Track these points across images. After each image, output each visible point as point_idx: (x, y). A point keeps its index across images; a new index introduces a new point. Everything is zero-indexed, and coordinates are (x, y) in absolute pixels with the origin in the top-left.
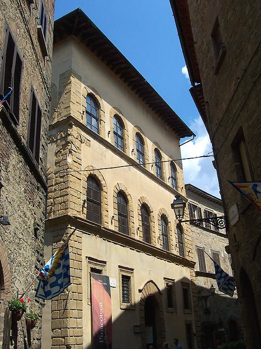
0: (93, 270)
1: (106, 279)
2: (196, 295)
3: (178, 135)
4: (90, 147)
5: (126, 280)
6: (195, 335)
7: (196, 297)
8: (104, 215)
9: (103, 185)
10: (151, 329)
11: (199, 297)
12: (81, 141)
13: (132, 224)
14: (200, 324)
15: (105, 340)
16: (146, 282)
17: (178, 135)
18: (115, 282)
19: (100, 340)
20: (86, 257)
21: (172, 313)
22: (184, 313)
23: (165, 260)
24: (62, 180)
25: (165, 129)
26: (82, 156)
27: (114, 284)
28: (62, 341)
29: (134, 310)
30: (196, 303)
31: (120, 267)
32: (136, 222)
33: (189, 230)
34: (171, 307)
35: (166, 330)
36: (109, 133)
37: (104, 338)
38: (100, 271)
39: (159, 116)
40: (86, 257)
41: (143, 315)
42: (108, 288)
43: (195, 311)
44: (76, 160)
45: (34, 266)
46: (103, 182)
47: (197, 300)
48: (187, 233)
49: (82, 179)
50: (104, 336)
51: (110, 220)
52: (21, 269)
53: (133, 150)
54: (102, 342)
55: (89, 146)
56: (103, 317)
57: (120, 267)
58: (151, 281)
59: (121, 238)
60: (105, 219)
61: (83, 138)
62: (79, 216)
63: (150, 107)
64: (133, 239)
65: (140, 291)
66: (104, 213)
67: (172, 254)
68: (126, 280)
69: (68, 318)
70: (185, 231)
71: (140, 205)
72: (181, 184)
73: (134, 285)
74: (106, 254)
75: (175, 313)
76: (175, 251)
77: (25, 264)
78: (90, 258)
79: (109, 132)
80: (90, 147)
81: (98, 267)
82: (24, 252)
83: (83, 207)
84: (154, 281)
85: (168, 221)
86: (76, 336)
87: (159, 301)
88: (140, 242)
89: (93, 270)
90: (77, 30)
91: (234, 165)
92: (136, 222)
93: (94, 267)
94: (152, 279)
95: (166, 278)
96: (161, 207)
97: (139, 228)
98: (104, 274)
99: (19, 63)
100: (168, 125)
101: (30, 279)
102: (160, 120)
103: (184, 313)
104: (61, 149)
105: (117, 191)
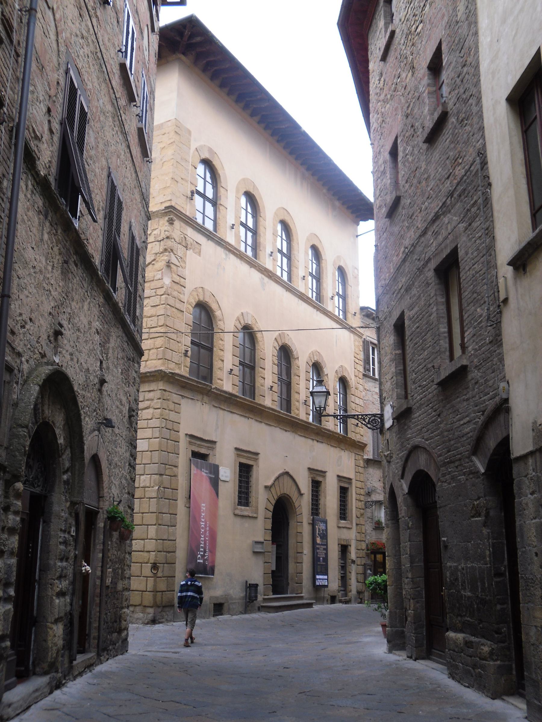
0: (195, 455)
1: (215, 470)
2: (362, 498)
4: (200, 255)
5: (245, 471)
6: (353, 562)
7: (361, 501)
8: (217, 367)
9: (218, 319)
11: (366, 502)
12: (186, 247)
13: (262, 381)
14: (364, 546)
15: (206, 560)
16: (277, 475)
17: (357, 217)
18: (227, 473)
19: (199, 559)
20: (186, 434)
22: (339, 527)
23: (313, 440)
25: (334, 208)
27: (226, 477)
29: (256, 518)
30: (362, 511)
32: (268, 374)
33: (361, 388)
37: (203, 556)
41: (269, 526)
42: (215, 482)
43: (357, 525)
44: (177, 279)
45: (127, 464)
46: (218, 313)
47: (363, 507)
48: (357, 393)
49: (184, 310)
50: (204, 554)
51: (226, 380)
52: (117, 471)
53: (272, 253)
54: (202, 561)
55: (199, 254)
58: (287, 473)
59: (244, 403)
60: (217, 373)
61: (189, 241)
62: (177, 371)
64: (260, 405)
66: (217, 364)
67: (325, 429)
68: (245, 471)
70: (353, 390)
72: (353, 308)
73: (257, 480)
77: (120, 464)
78: (192, 436)
79: (233, 225)
80: (200, 255)
81: (203, 451)
82: (120, 449)
83: (186, 354)
84: (291, 473)
85: (323, 372)
87: (296, 505)
88: (273, 410)
89: (195, 455)
90: (191, 47)
91: (394, 353)
92: (268, 374)
93: (196, 449)
94: (287, 470)
95: (313, 470)
96: (313, 349)
97: (272, 387)
98: (211, 460)
99: (120, 203)
101: (124, 481)
103: (339, 527)
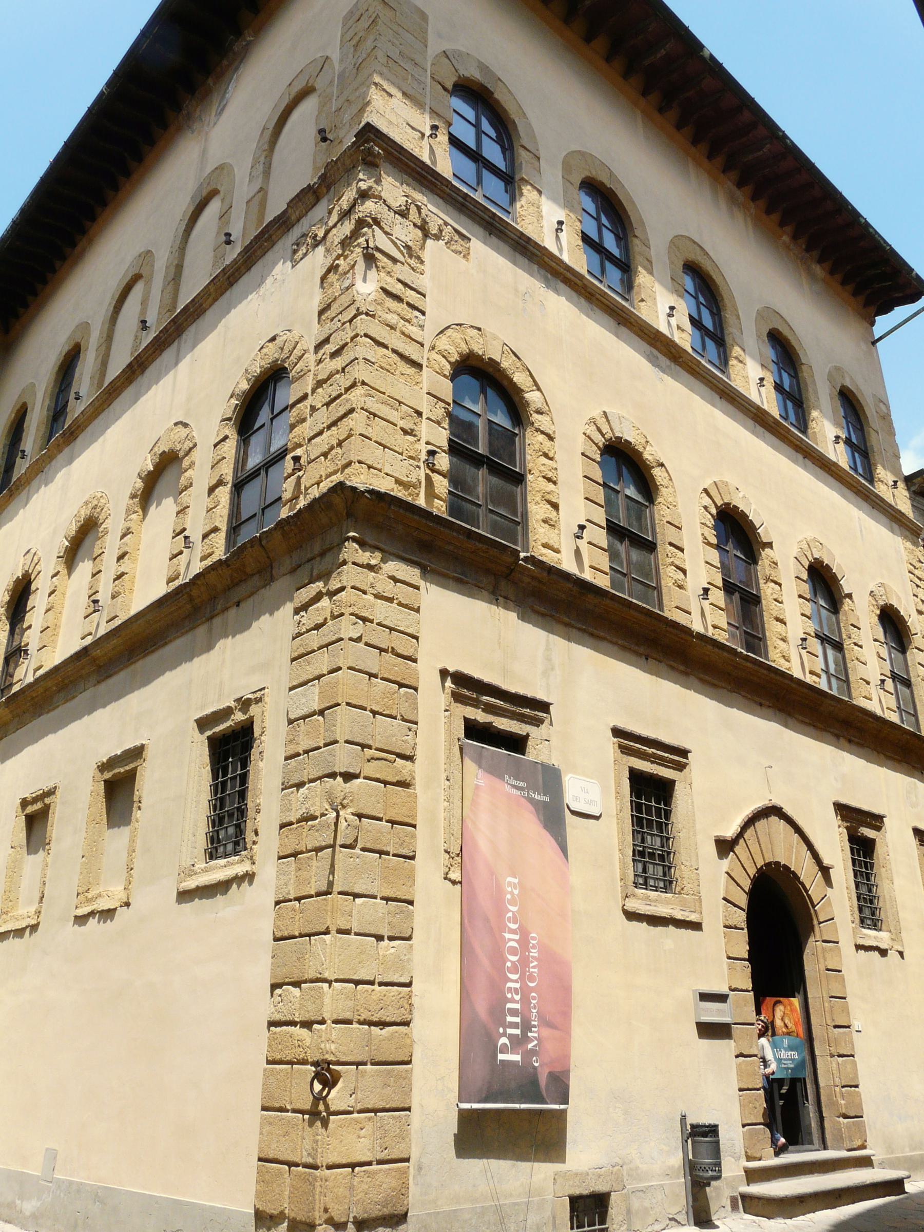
1: (550, 780)
3: (866, 305)
9: (532, 408)
10: (315, 1026)
15: (533, 1052)
17: (866, 305)
19: (504, 1049)
20: (444, 673)
21: (883, 953)
24: (338, 363)
26: (424, 282)
27: (590, 802)
28: (300, 1042)
31: (617, 732)
34: (875, 924)
35: (856, 1024)
36: (559, 230)
38: (517, 744)
39: (782, 224)
40: (444, 673)
41: (743, 949)
42: (553, 816)
46: (533, 397)
50: (524, 1033)
54: (517, 1058)
56: (524, 942)
57: (617, 732)
63: (740, 184)
65: (725, 847)
69: (327, 932)
71: (714, 511)
74: (546, 674)
75: (186, 533)
76: (878, 701)
79: (560, 223)
80: (467, 260)
84: (789, 810)
85: (839, 588)
86: (371, 1024)
89: (474, 731)
93: (481, 716)
95: (607, 417)
98: (536, 752)
100: (820, 261)
102: (785, 238)
104: (338, 258)
105: (601, 441)
